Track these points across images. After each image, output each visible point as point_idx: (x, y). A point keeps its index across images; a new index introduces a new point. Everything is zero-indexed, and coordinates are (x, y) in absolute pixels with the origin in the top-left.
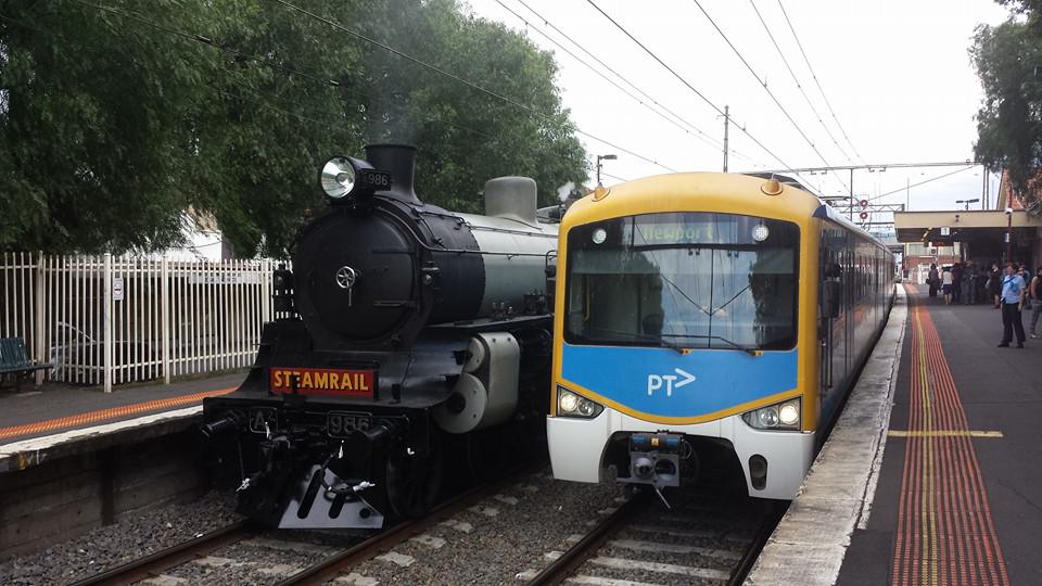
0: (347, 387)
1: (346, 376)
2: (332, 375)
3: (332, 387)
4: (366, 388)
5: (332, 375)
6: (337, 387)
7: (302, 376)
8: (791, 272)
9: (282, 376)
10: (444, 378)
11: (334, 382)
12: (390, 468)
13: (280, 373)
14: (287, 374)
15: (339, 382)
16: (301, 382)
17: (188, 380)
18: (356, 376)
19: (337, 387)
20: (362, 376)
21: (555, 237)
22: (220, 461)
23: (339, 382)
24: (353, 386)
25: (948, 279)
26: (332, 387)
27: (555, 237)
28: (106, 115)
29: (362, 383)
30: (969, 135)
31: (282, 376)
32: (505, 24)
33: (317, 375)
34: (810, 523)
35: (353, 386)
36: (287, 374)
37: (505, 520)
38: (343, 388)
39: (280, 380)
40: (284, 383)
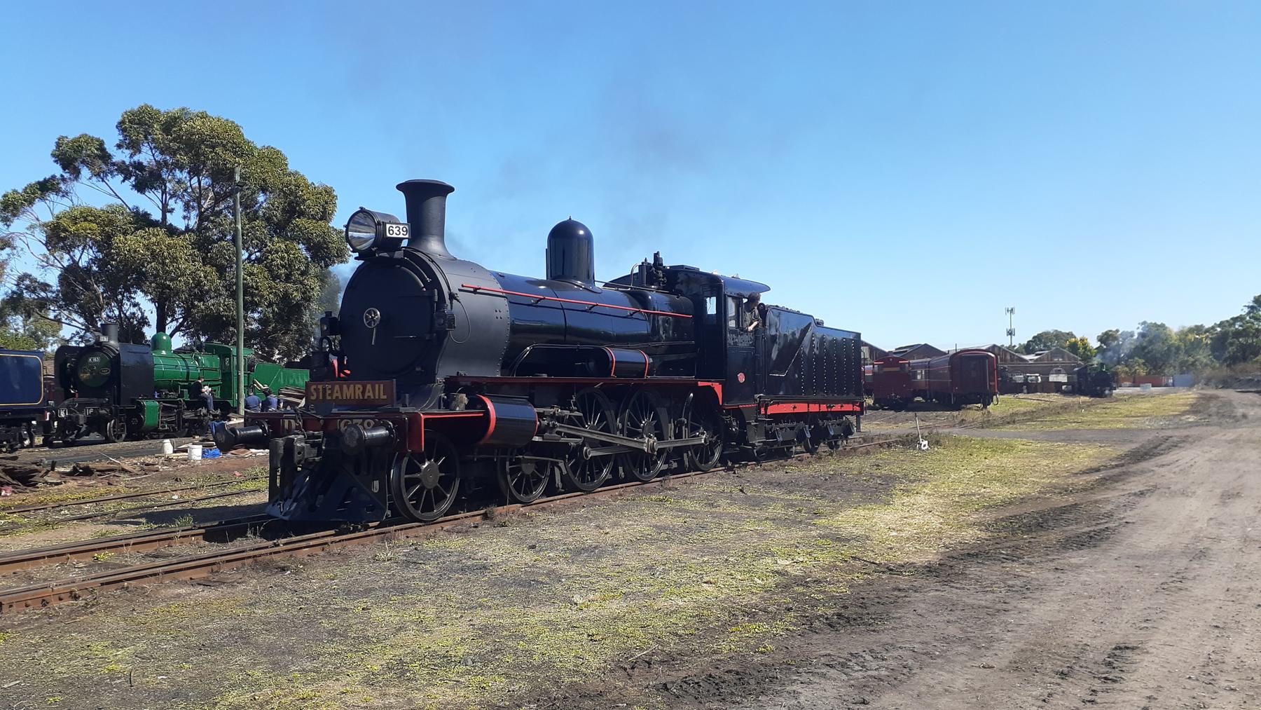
0: (337, 397)
3: (357, 398)
4: (385, 397)
7: (332, 389)
8: (202, 536)
9: (317, 390)
10: (1141, 385)
11: (359, 392)
13: (315, 387)
14: (320, 387)
15: (363, 393)
16: (330, 395)
18: (377, 386)
19: (361, 398)
20: (382, 386)
21: (355, 387)
23: (363, 393)
24: (374, 396)
27: (355, 387)
29: (382, 392)
30: (1059, 330)
32: (3, 194)
34: (1179, 405)
35: (374, 396)
37: (312, 234)
39: (315, 394)
40: (318, 397)
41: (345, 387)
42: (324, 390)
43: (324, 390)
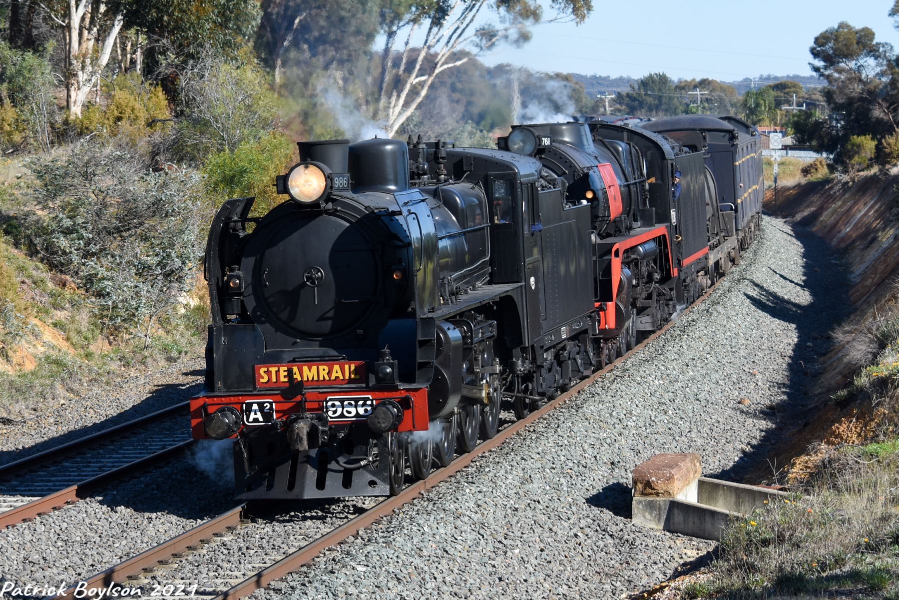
1: (336, 367)
2: (321, 368)
3: (321, 378)
5: (321, 368)
6: (327, 378)
9: (268, 372)
12: (827, 187)
13: (265, 369)
15: (329, 373)
17: (461, 314)
19: (327, 378)
22: (389, 370)
23: (329, 373)
24: (344, 375)
25: (820, 63)
26: (321, 378)
28: (379, 43)
31: (268, 372)
33: (305, 369)
35: (344, 375)
36: (273, 370)
38: (333, 378)
41: (305, 369)
42: (278, 372)
43: (278, 372)
